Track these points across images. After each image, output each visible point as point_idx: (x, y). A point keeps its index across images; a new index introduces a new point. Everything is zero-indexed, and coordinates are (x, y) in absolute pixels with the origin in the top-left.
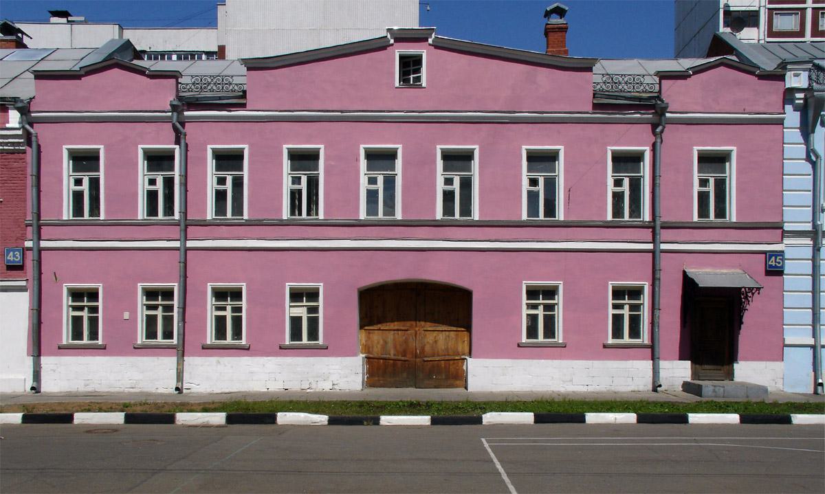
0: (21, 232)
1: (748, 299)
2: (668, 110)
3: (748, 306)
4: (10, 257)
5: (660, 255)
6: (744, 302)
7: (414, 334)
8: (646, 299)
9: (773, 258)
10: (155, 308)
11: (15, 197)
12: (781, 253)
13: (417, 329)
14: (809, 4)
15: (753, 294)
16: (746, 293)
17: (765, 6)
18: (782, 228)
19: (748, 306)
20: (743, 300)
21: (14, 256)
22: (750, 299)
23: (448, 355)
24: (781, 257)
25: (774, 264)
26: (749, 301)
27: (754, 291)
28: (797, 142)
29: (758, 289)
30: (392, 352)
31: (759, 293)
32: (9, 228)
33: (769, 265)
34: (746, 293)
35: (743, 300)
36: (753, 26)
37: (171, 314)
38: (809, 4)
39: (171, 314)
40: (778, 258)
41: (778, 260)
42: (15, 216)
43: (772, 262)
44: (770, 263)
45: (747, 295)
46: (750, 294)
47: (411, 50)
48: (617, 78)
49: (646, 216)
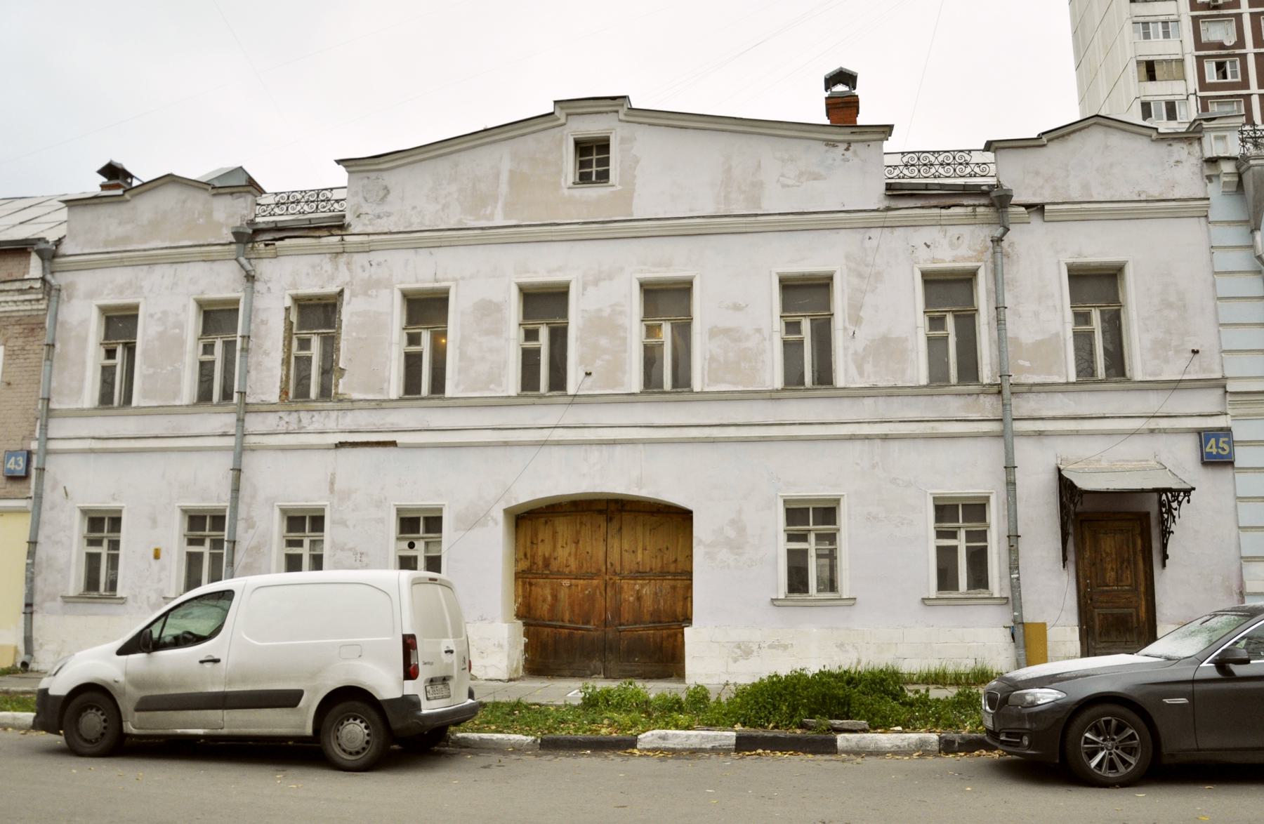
0: (30, 428)
1: (1172, 514)
2: (1014, 200)
3: (1173, 525)
4: (11, 465)
5: (1250, 218)
6: (1167, 520)
7: (603, 588)
8: (995, 515)
9: (1213, 441)
10: (200, 542)
11: (26, 378)
12: (1227, 431)
13: (607, 578)
14: (1245, 9)
15: (1180, 503)
16: (1169, 502)
17: (1195, 94)
18: (1224, 387)
19: (1173, 525)
20: (1166, 516)
21: (16, 463)
22: (1175, 513)
23: (660, 622)
24: (1226, 439)
25: (1214, 451)
26: (1174, 517)
27: (1180, 499)
28: (1251, 322)
29: (1188, 492)
30: (567, 617)
31: (1189, 501)
32: (15, 423)
33: (1207, 453)
34: (1169, 502)
35: (1166, 516)
36: (1154, 65)
37: (220, 551)
38: (1245, 9)
39: (220, 551)
40: (1222, 440)
41: (1221, 445)
42: (24, 405)
43: (1211, 448)
44: (1208, 450)
45: (1170, 507)
46: (1175, 505)
47: (591, 127)
48: (926, 157)
49: (987, 373)
